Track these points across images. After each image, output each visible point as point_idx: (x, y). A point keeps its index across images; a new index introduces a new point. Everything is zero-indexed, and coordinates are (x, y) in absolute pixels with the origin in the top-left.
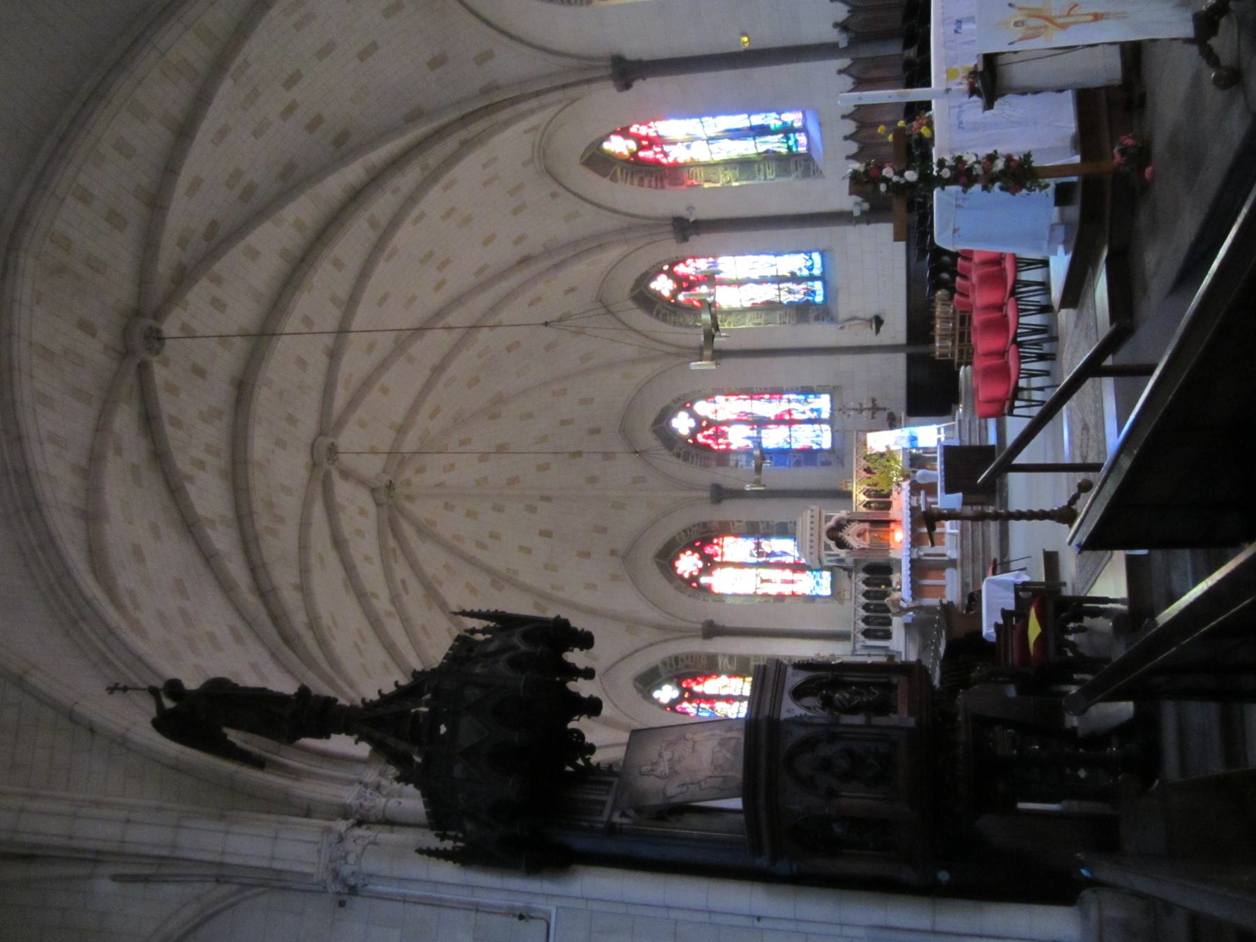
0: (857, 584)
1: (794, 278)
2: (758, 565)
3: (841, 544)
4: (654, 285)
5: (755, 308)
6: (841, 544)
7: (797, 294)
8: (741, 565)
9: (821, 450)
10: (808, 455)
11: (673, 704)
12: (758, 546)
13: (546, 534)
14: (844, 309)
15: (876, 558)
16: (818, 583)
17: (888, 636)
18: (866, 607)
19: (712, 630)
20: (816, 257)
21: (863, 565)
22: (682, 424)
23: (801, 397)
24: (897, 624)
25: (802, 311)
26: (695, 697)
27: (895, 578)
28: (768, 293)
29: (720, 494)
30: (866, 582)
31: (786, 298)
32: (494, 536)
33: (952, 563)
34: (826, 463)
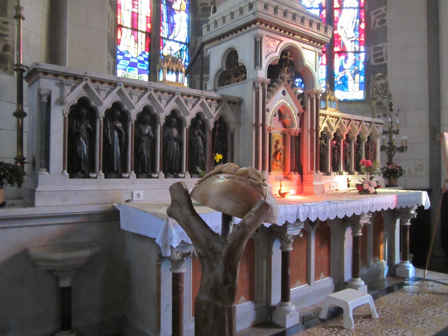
16: (133, 65)
17: (77, 166)
18: (174, 119)
21: (230, 117)
23: (361, 67)
30: (199, 121)
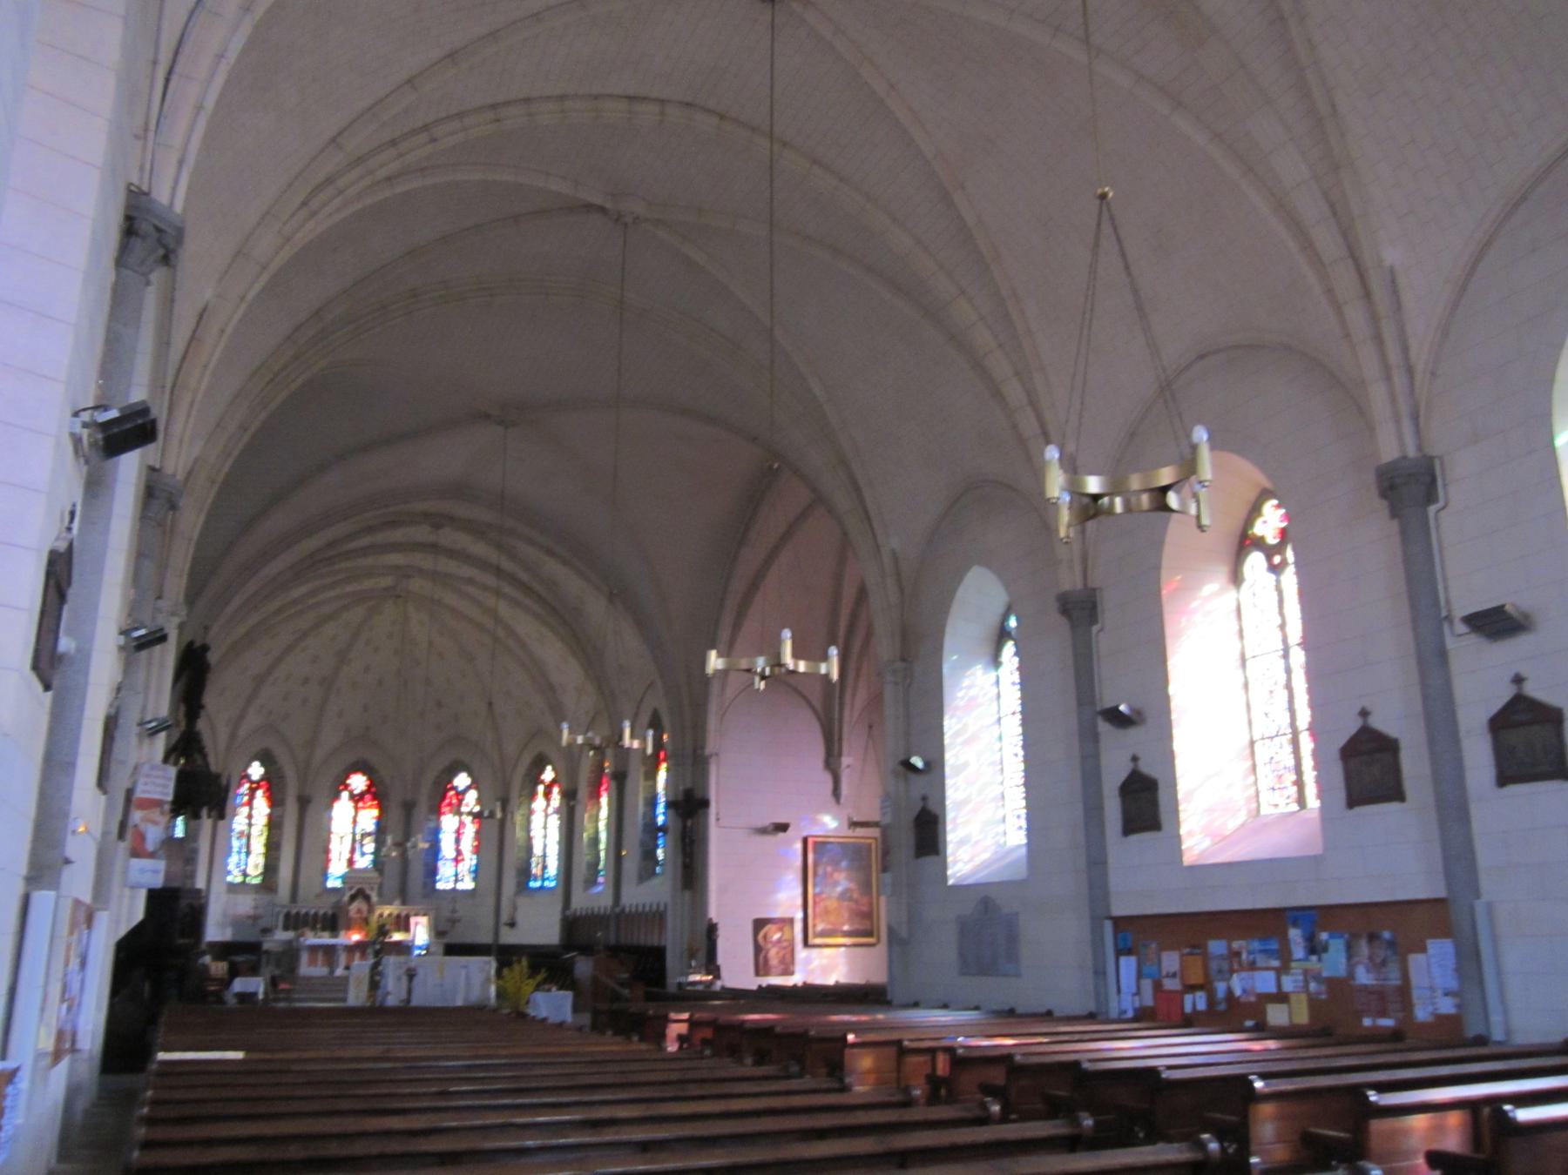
0: (324, 907)
1: (544, 867)
2: (354, 834)
3: (353, 898)
4: (549, 768)
5: (529, 839)
6: (353, 898)
7: (536, 870)
8: (355, 822)
9: (435, 882)
10: (432, 872)
11: (247, 777)
12: (369, 834)
13: (380, 683)
14: (523, 902)
15: (341, 921)
17: (286, 928)
19: (304, 802)
20: (553, 884)
22: (462, 780)
24: (290, 935)
25: (525, 873)
26: (252, 792)
27: (326, 934)
28: (537, 850)
29: (409, 807)
31: (534, 860)
32: (376, 650)
33: (332, 972)
34: (425, 885)
